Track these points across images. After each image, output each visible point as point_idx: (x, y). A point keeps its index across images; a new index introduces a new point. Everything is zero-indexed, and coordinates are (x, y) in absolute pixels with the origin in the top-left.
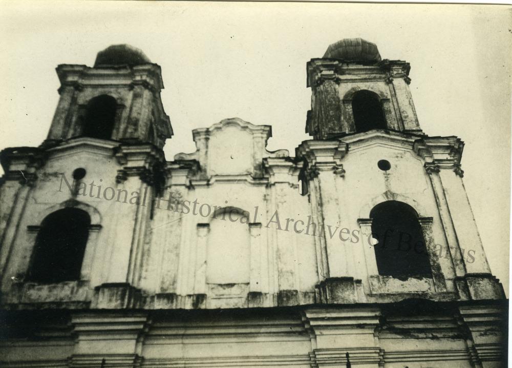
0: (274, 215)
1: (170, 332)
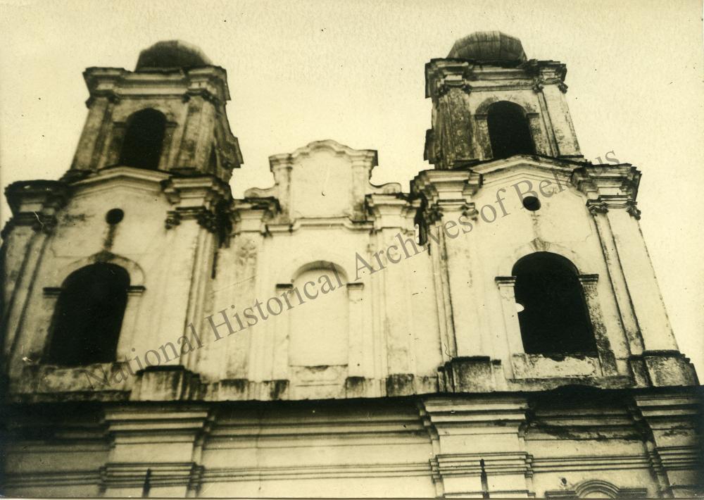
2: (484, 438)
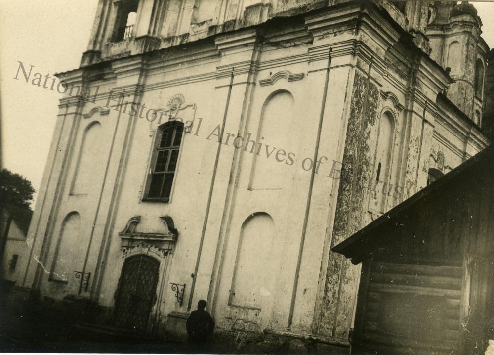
0: (216, 128)
1: (155, 66)
2: (238, 55)
